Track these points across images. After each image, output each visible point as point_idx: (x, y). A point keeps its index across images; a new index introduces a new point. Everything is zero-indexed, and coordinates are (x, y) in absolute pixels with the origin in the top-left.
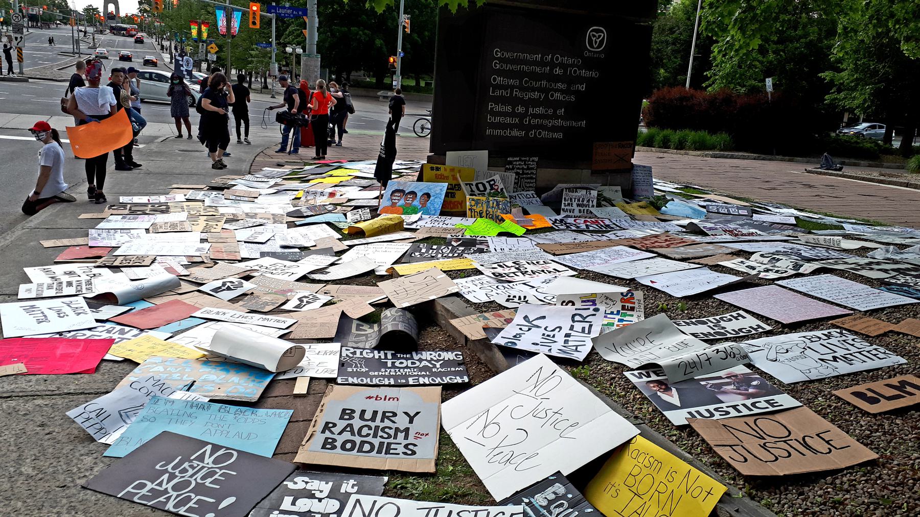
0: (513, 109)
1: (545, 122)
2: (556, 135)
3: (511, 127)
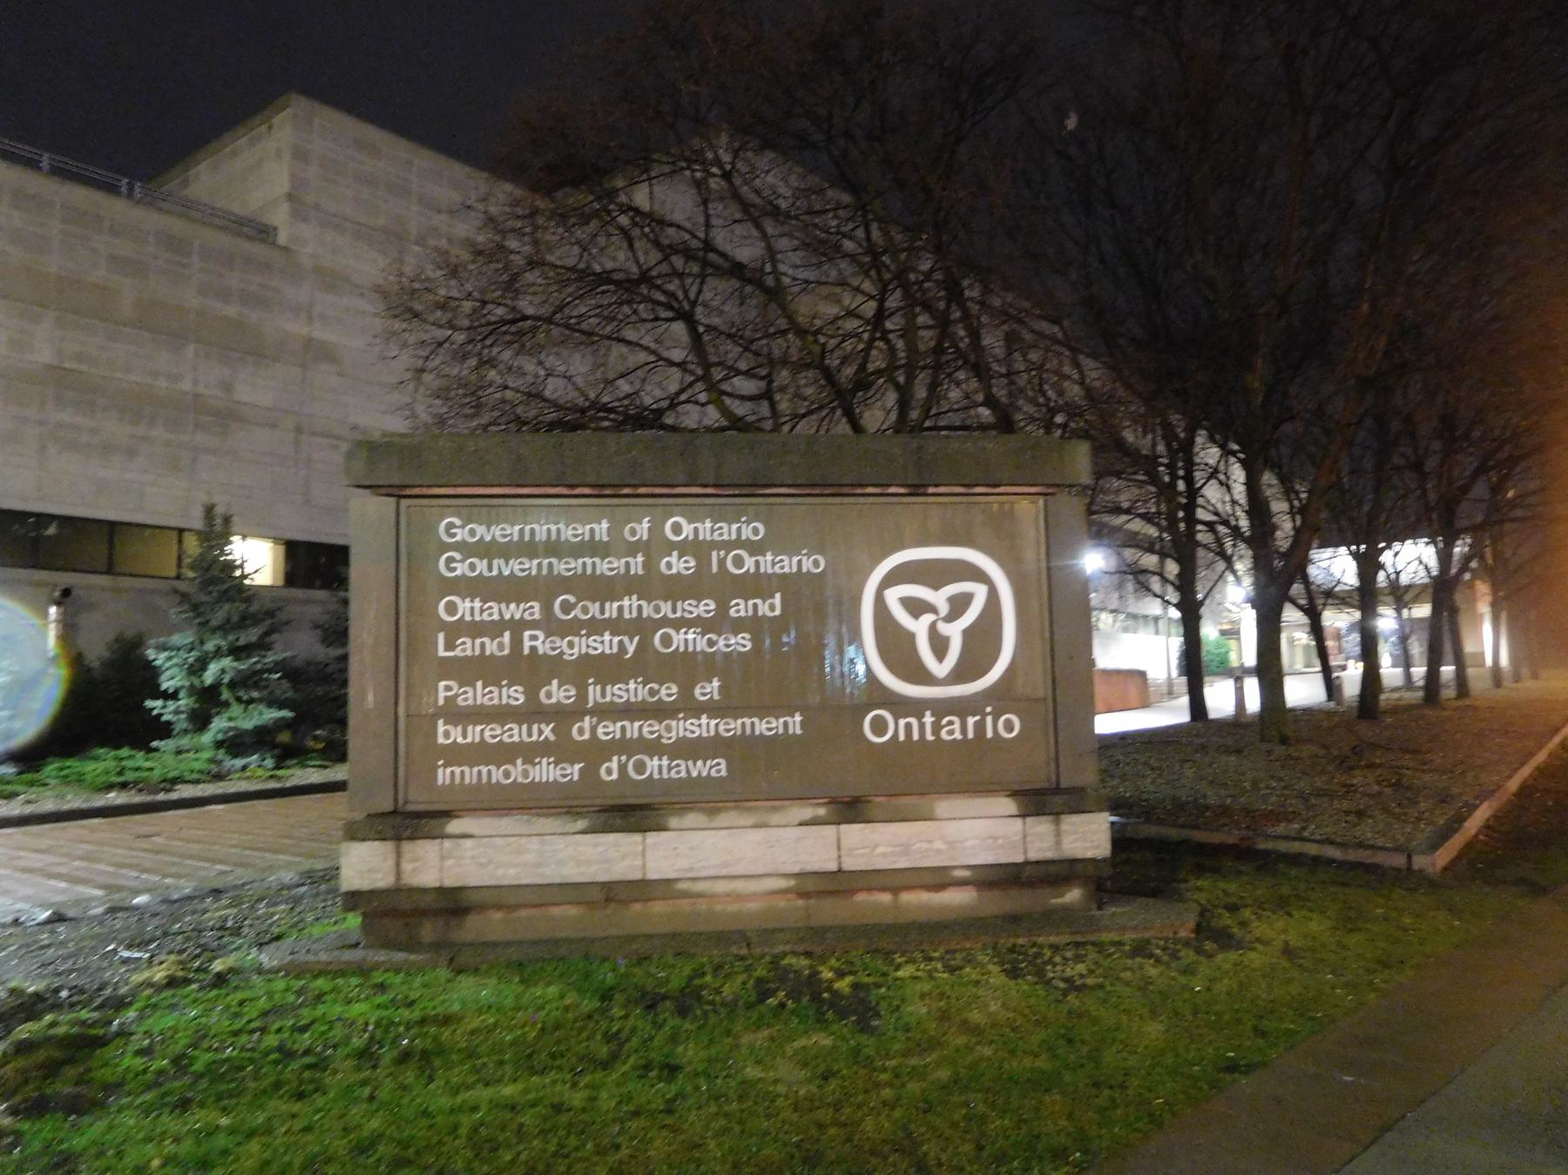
0: (532, 694)
1: (648, 729)
2: (699, 769)
3: (530, 753)
